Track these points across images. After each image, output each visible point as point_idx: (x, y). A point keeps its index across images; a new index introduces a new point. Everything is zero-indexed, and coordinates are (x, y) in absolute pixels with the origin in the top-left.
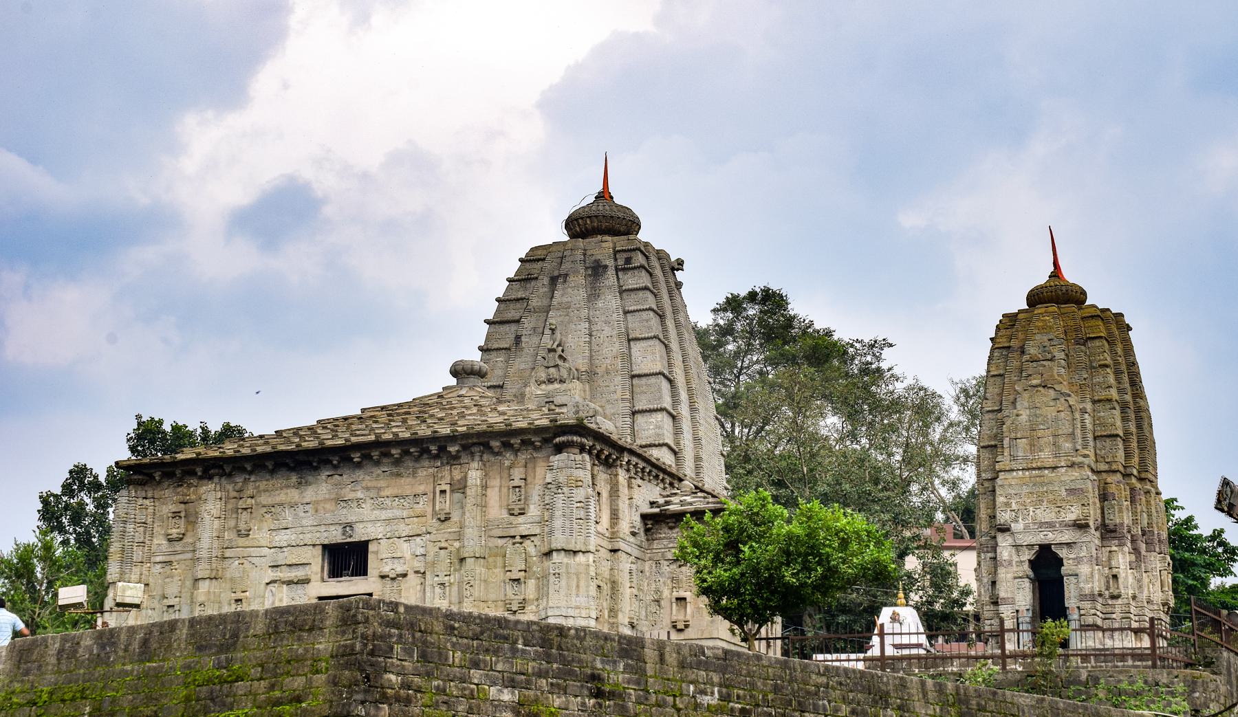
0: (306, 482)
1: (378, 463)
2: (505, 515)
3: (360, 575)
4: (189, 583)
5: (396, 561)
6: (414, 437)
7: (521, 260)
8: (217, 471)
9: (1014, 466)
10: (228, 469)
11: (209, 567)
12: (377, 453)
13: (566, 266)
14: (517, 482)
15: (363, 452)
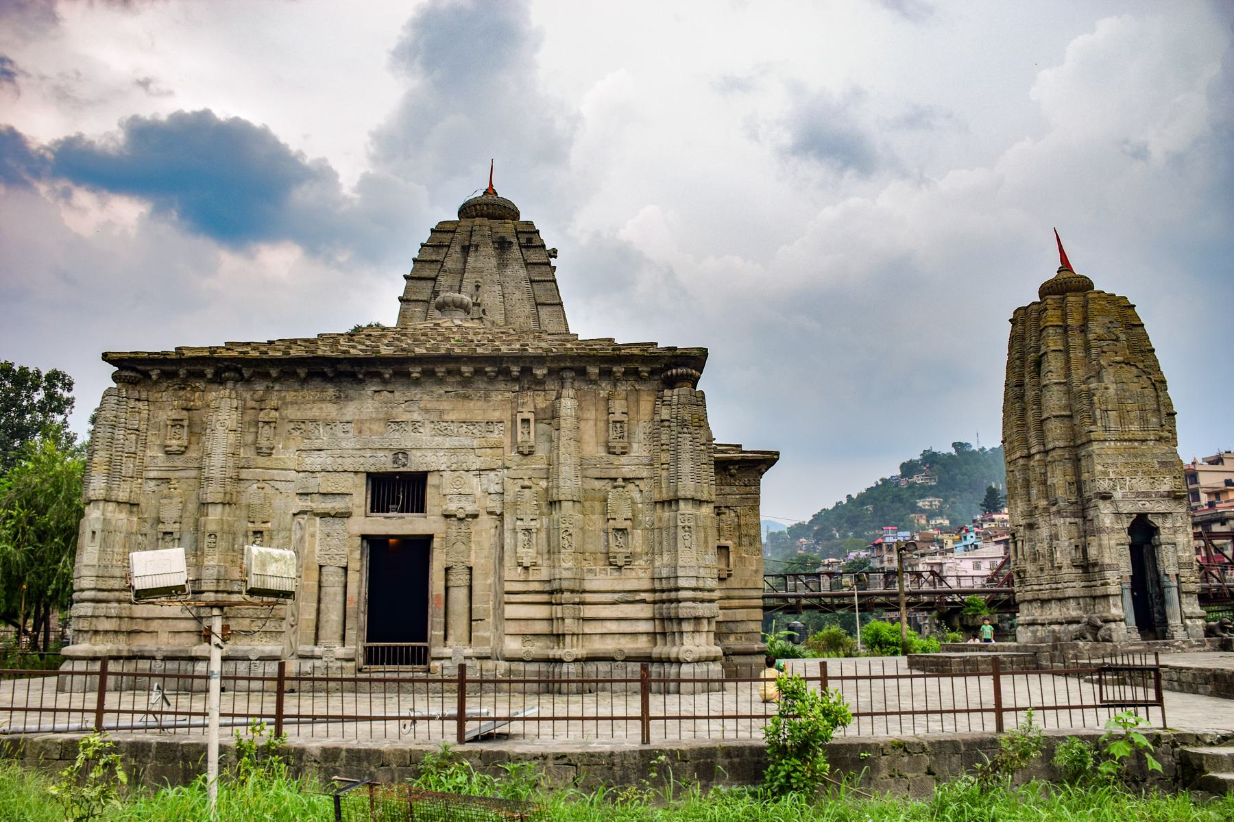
0: (346, 397)
1: (441, 382)
2: (602, 452)
3: (412, 512)
4: (192, 507)
5: (463, 498)
6: (496, 353)
7: (432, 231)
8: (232, 374)
9: (1107, 436)
10: (246, 373)
11: (221, 490)
12: (443, 369)
13: (475, 239)
14: (618, 417)
15: (425, 367)
